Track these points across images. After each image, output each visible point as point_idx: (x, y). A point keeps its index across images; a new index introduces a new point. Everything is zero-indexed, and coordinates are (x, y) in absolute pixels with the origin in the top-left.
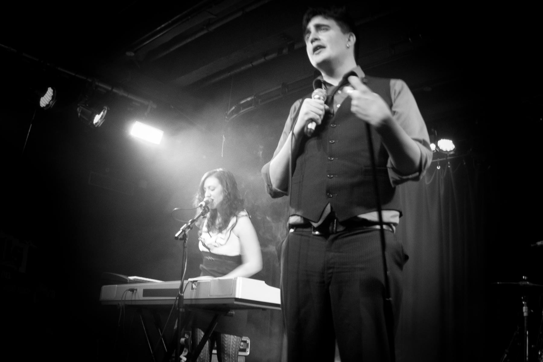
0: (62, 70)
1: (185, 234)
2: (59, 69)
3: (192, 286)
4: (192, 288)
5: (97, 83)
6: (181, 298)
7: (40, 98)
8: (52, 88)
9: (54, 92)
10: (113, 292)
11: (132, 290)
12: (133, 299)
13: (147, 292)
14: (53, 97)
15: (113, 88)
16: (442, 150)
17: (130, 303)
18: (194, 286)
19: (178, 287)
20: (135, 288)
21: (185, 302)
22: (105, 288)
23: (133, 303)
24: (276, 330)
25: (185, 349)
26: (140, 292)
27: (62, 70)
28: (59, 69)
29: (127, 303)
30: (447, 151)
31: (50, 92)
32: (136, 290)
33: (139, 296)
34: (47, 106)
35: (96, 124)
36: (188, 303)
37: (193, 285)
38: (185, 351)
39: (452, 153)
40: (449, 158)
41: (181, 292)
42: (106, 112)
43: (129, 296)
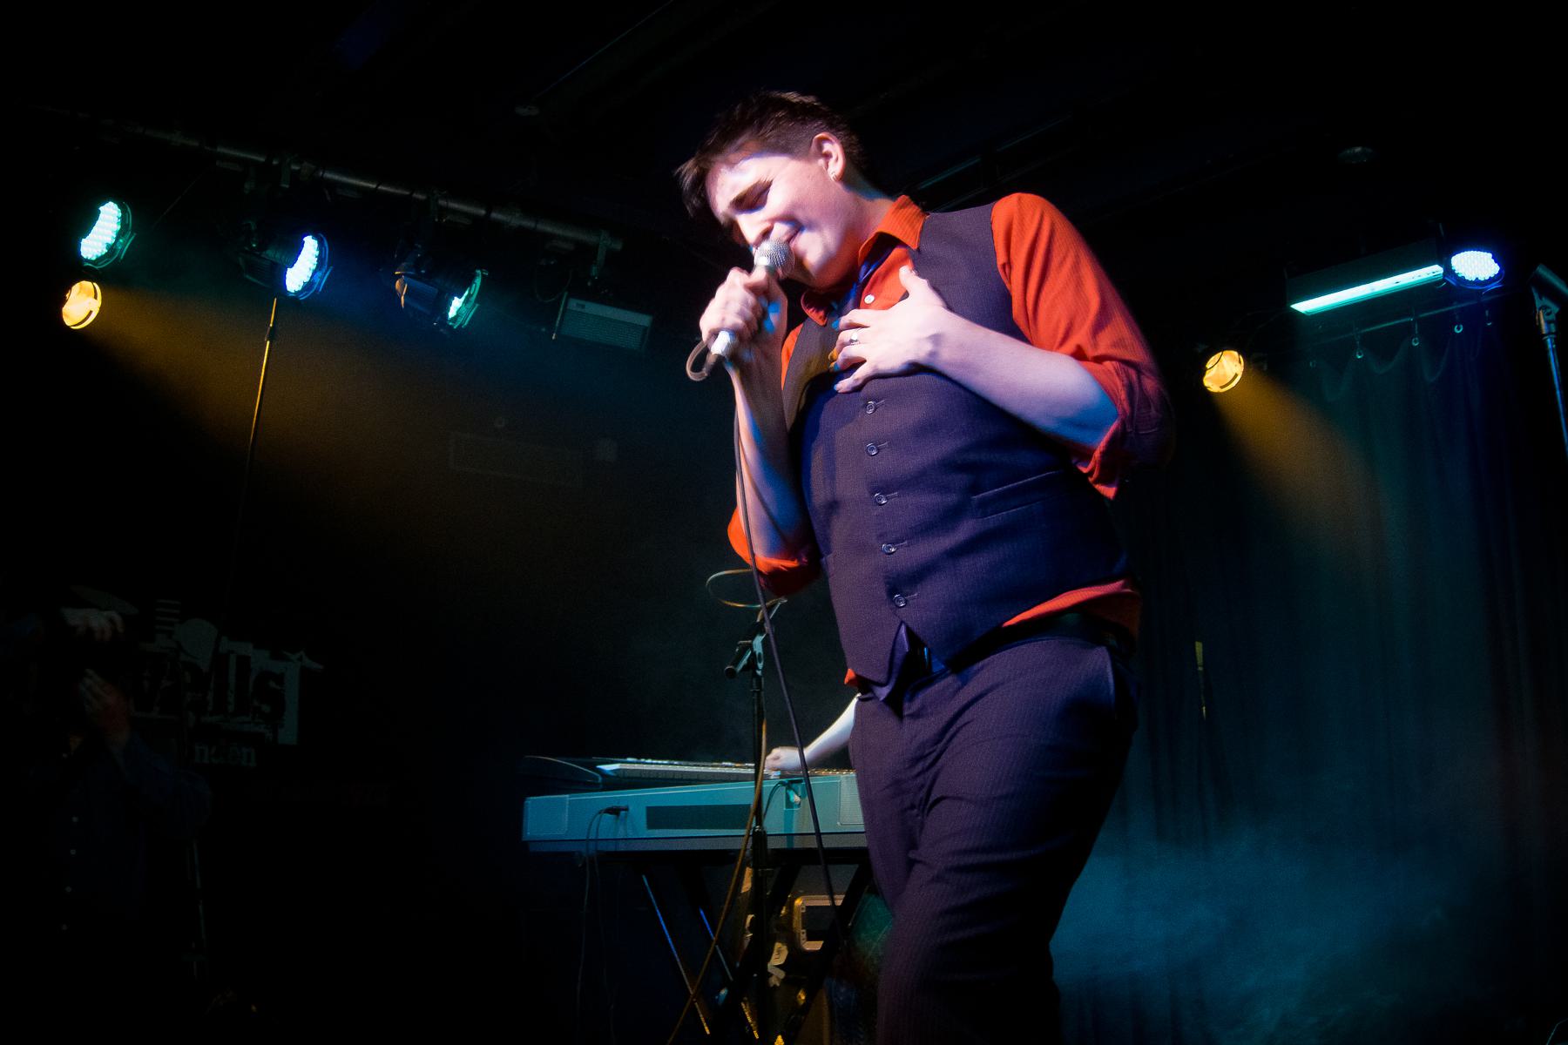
0: (336, 177)
1: (753, 654)
2: (328, 175)
3: (788, 797)
4: (789, 804)
5: (442, 202)
6: (760, 838)
7: (68, 288)
8: (316, 236)
9: (321, 247)
10: (553, 818)
11: (615, 811)
12: (621, 835)
13: (658, 817)
14: (320, 259)
15: (489, 211)
16: (1463, 280)
17: (611, 848)
18: (795, 798)
19: (751, 800)
20: (622, 805)
21: (772, 844)
22: (536, 806)
23: (622, 847)
24: (867, 203)
25: (778, 945)
26: (639, 817)
27: (336, 177)
28: (328, 175)
29: (603, 847)
30: (1477, 282)
31: (310, 245)
32: (626, 809)
33: (636, 831)
34: (308, 286)
35: (455, 319)
36: (781, 844)
37: (791, 793)
38: (779, 952)
39: (1493, 286)
40: (1486, 299)
41: (759, 822)
42: (478, 281)
43: (608, 828)
